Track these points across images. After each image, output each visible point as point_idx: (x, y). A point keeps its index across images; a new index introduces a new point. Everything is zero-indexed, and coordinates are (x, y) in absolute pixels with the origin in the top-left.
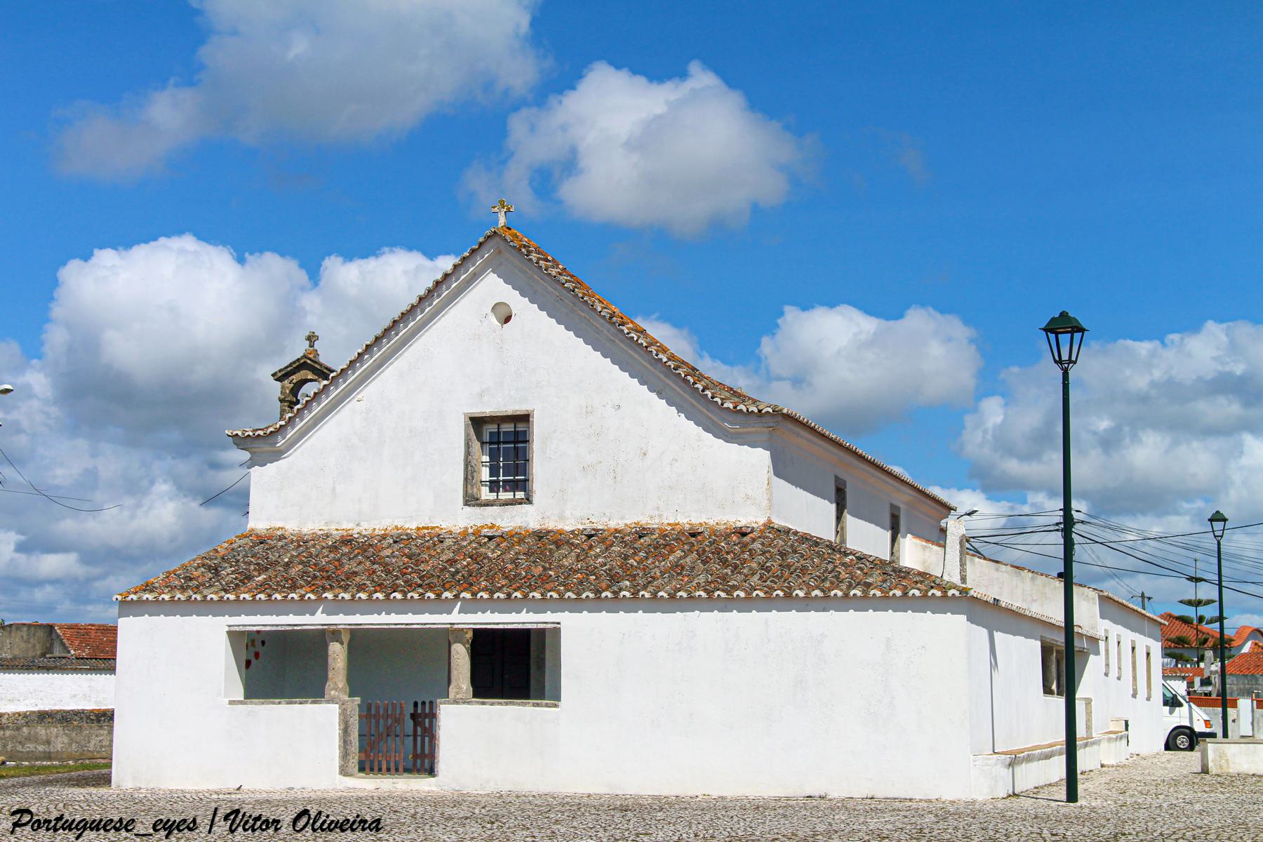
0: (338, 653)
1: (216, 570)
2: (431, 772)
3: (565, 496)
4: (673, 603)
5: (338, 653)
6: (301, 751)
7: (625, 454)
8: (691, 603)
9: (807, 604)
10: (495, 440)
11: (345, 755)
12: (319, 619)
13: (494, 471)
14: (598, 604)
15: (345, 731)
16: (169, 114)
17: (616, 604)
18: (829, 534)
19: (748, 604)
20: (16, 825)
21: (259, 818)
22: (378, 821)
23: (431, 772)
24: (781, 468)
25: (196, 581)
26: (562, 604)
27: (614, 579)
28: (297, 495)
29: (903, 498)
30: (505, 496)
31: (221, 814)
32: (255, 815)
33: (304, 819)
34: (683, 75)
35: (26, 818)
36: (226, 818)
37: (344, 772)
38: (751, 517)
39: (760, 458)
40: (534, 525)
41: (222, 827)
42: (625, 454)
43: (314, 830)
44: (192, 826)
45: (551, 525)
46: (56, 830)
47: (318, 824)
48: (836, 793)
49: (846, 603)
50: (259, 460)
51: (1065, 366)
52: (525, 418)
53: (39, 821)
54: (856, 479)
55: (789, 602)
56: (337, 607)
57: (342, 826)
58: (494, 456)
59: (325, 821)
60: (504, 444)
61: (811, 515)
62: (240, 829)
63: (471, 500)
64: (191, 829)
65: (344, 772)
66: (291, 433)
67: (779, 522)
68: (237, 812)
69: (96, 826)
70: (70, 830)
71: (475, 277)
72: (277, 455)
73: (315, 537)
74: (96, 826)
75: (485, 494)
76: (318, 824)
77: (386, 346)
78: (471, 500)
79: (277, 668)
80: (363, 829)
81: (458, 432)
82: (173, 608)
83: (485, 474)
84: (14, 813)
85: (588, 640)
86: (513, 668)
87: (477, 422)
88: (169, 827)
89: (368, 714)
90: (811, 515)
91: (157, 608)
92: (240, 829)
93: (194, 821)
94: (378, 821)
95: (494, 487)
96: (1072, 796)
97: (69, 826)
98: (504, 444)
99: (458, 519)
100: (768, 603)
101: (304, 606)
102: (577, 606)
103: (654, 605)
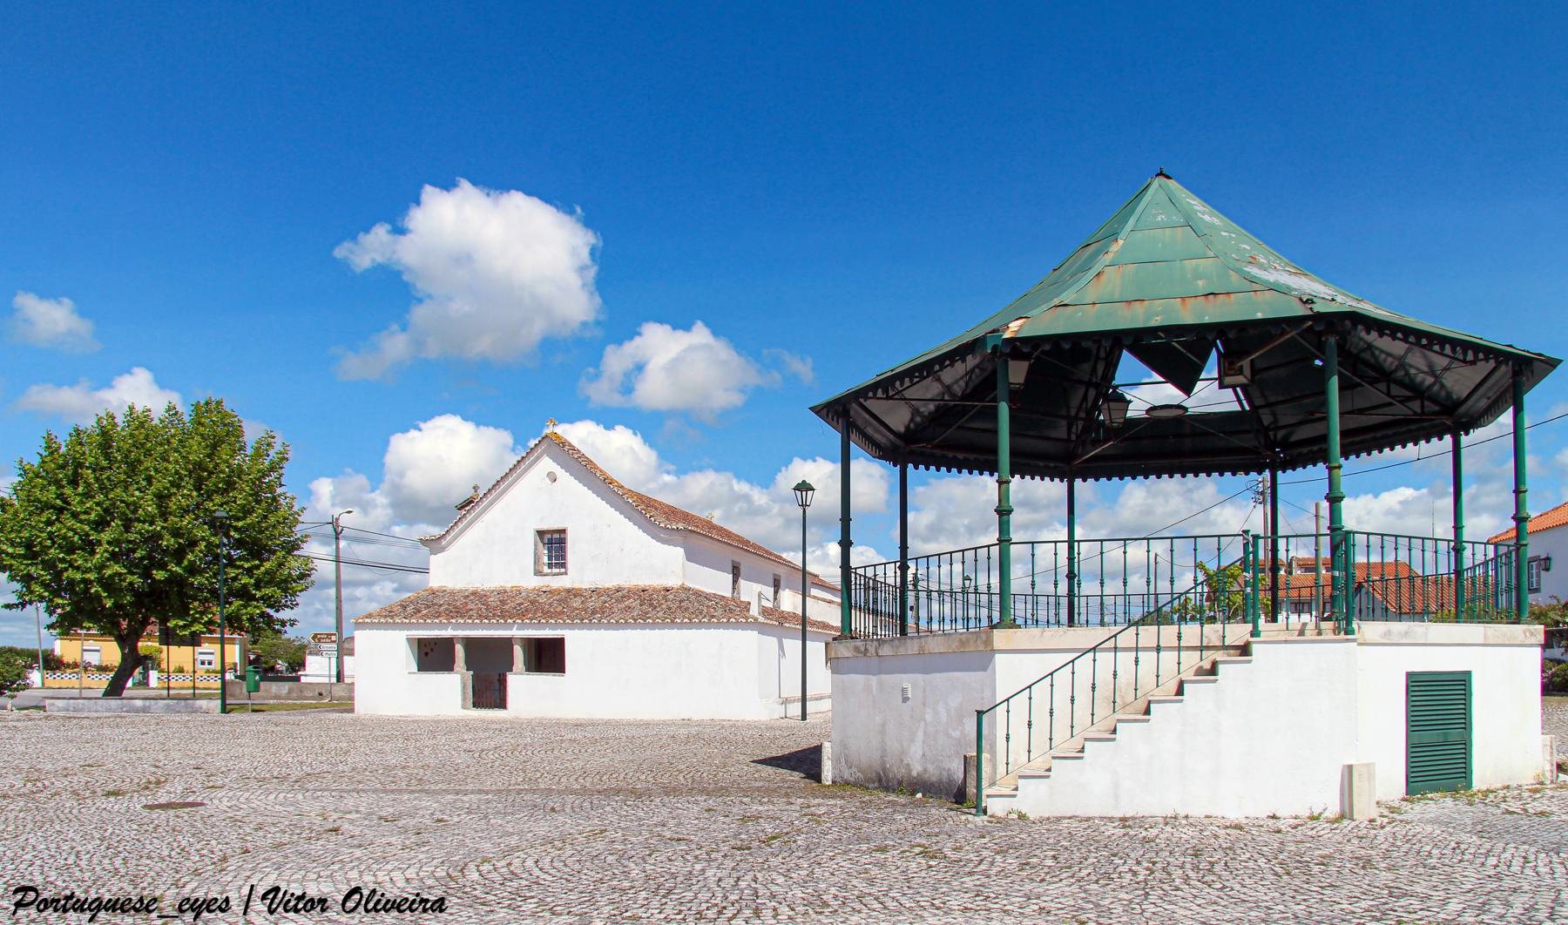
0: (459, 650)
1: (405, 607)
2: (502, 704)
3: (585, 571)
4: (618, 626)
5: (459, 650)
6: (446, 692)
7: (615, 553)
8: (626, 626)
9: (682, 626)
10: (550, 542)
11: (464, 699)
12: (448, 633)
13: (550, 558)
14: (582, 626)
15: (464, 687)
16: (396, 345)
17: (590, 626)
18: (727, 593)
19: (654, 626)
20: (19, 905)
21: (302, 897)
22: (442, 900)
23: (502, 704)
24: (691, 557)
25: (389, 617)
26: (565, 626)
27: (594, 612)
28: (449, 571)
29: (781, 571)
30: (555, 570)
31: (261, 891)
32: (299, 893)
33: (357, 896)
34: (687, 327)
35: (32, 896)
36: (264, 897)
37: (464, 707)
38: (673, 582)
39: (680, 551)
40: (568, 586)
41: (258, 906)
42: (615, 553)
43: (367, 911)
44: (225, 907)
45: (577, 586)
46: (65, 911)
47: (371, 905)
48: (695, 718)
49: (701, 625)
50: (434, 552)
51: (804, 506)
52: (564, 531)
53: (45, 900)
54: (746, 562)
55: (673, 624)
56: (457, 627)
57: (396, 906)
58: (550, 550)
59: (379, 901)
60: (554, 543)
61: (716, 582)
62: (280, 909)
63: (538, 573)
64: (223, 911)
65: (464, 707)
66: (449, 538)
67: (689, 584)
68: (277, 889)
69: (114, 906)
70: (83, 910)
71: (538, 458)
72: (442, 549)
73: (460, 591)
74: (114, 906)
75: (546, 570)
76: (371, 905)
77: (494, 493)
78: (538, 573)
79: (433, 656)
80: (425, 910)
81: (530, 538)
82: (379, 626)
83: (546, 560)
84: (15, 892)
85: (577, 643)
86: (547, 657)
87: (541, 533)
88: (198, 907)
89: (476, 680)
90: (716, 582)
91: (372, 626)
92: (280, 909)
93: (227, 900)
94: (442, 900)
95: (550, 566)
96: (804, 717)
97: (80, 907)
98: (554, 543)
99: (531, 582)
100: (663, 626)
101: (441, 626)
102: (572, 626)
103: (609, 626)
